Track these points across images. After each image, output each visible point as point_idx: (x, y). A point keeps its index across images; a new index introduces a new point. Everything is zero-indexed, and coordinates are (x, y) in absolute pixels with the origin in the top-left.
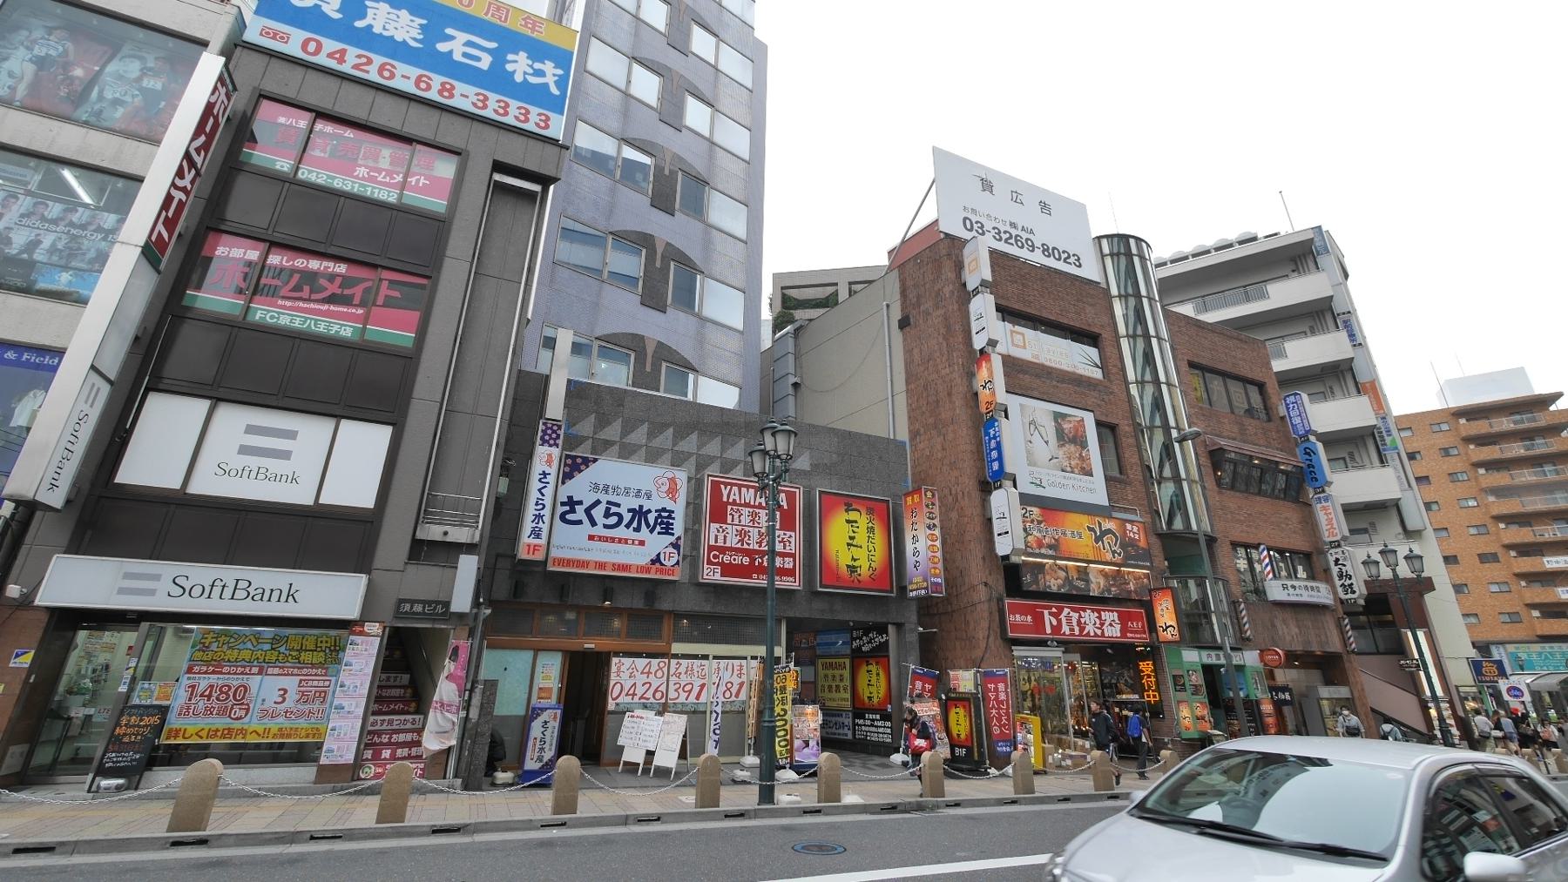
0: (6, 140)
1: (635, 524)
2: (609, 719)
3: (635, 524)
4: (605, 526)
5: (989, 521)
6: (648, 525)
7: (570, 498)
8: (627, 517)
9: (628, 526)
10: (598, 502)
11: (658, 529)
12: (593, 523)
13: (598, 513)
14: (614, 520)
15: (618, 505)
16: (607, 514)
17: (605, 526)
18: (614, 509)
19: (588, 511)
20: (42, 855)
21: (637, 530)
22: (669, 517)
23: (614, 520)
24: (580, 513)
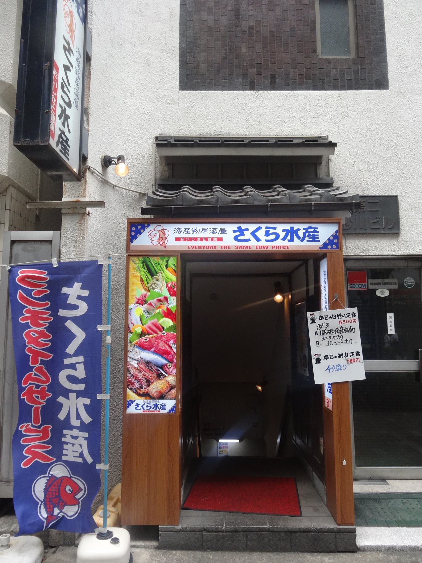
0: (90, 1)
1: (289, 238)
2: (129, 311)
3: (289, 238)
4: (267, 241)
5: (123, 471)
6: (298, 237)
9: (284, 239)
11: (307, 239)
13: (145, 406)
14: (149, 408)
16: (147, 406)
17: (267, 241)
18: (271, 231)
19: (142, 406)
20: (309, 278)
21: (292, 240)
22: (315, 231)
23: (149, 408)
24: (140, 407)
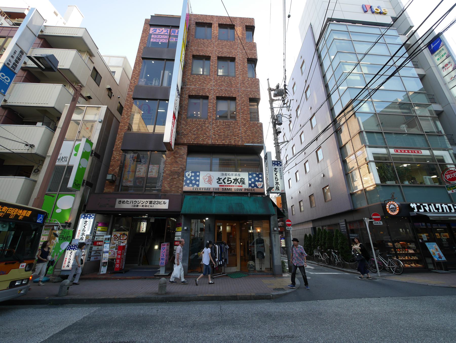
8: (233, 181)
10: (225, 178)
12: (225, 183)
13: (226, 181)
14: (230, 182)
16: (228, 181)
19: (223, 180)
23: (230, 182)
24: (221, 181)
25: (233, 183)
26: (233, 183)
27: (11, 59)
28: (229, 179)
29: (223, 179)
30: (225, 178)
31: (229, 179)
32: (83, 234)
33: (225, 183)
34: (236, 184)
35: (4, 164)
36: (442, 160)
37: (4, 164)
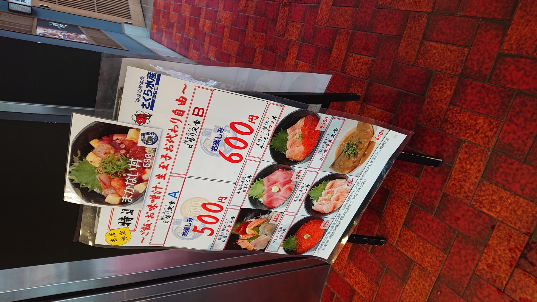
1: (151, 86)
3: (151, 86)
6: (152, 82)
7: (142, 105)
10: (143, 97)
12: (150, 99)
13: (147, 97)
14: (149, 93)
15: (145, 91)
16: (148, 95)
19: (146, 100)
23: (149, 93)
24: (147, 103)
25: (152, 88)
26: (152, 88)
27: (222, 240)
28: (146, 92)
29: (144, 101)
30: (143, 97)
31: (146, 92)
32: (151, 207)
33: (150, 99)
34: (153, 85)
35: (321, 105)
36: (334, 294)
37: (321, 105)
